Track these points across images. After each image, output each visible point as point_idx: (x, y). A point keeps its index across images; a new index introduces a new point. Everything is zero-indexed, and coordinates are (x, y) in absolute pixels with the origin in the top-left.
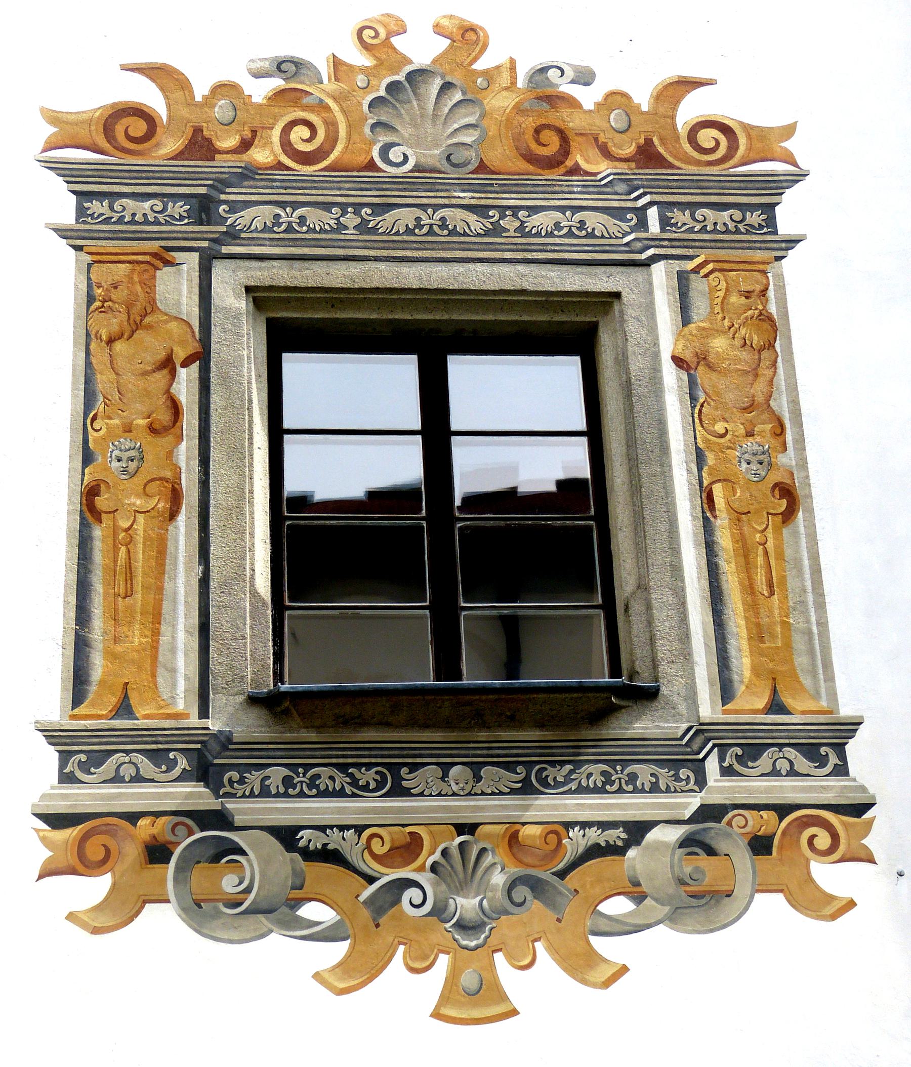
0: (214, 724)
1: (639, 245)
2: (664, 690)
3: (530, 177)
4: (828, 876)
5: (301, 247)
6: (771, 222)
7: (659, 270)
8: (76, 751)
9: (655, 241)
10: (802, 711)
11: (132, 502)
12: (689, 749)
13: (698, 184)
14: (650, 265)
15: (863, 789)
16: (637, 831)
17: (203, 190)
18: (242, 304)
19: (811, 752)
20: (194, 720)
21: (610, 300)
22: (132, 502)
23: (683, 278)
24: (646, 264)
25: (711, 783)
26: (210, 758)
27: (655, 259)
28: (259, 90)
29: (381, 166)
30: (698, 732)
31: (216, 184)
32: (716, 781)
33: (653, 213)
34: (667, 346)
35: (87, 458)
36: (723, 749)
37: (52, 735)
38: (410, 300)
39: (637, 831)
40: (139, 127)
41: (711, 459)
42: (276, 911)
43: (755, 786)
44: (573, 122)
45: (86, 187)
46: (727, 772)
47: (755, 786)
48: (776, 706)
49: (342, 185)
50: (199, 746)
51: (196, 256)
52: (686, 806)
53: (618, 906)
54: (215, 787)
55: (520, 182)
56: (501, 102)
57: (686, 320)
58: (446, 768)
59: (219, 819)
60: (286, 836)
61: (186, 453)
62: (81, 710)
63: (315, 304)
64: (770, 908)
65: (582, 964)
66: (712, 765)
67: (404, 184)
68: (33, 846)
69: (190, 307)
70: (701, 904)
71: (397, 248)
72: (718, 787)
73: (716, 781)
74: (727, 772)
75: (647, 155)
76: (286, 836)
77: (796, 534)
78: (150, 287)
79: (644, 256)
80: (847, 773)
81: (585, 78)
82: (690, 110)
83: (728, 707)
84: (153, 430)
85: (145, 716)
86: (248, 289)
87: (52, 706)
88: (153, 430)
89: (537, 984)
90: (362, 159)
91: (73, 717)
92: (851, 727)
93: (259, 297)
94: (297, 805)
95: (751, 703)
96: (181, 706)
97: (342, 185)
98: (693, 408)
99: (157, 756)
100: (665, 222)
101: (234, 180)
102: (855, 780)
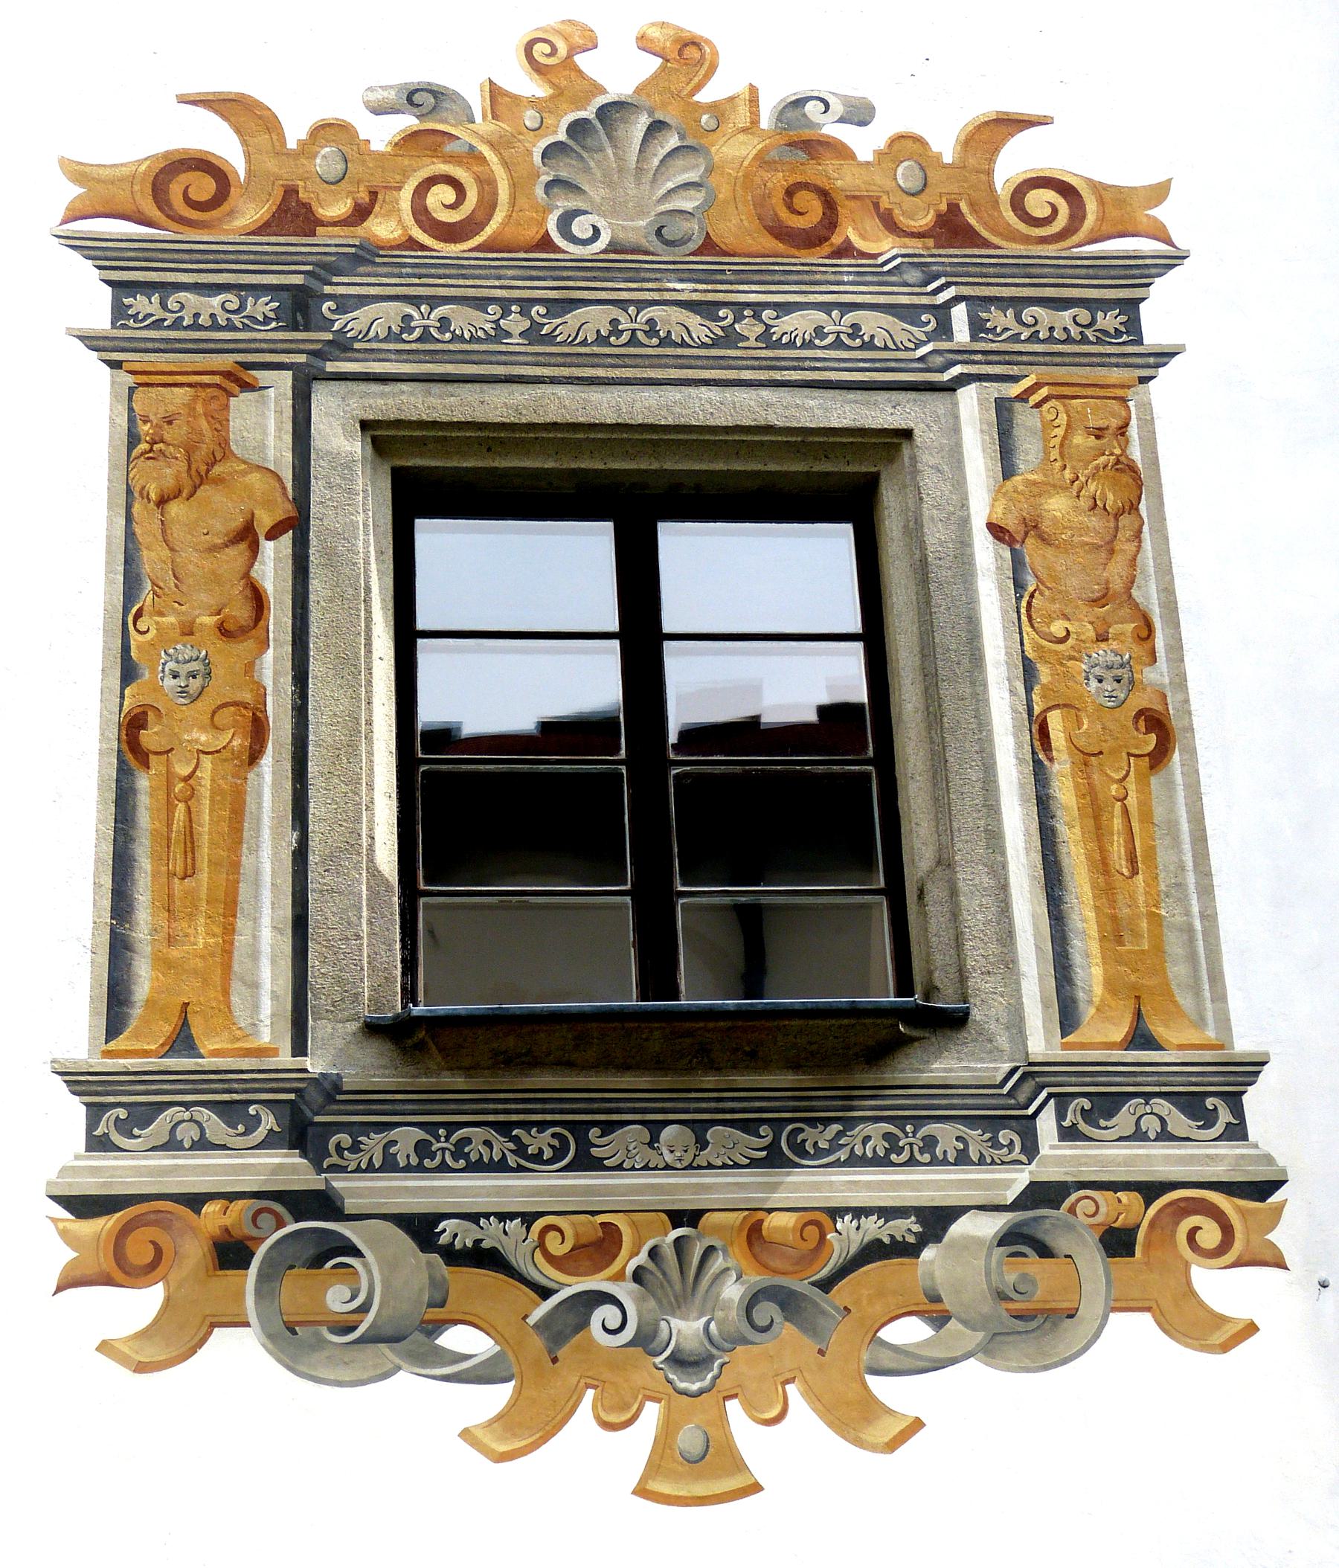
0: (315, 1065)
1: (939, 360)
2: (976, 1014)
3: (779, 260)
4: (1218, 1287)
5: (442, 363)
6: (1133, 326)
7: (968, 397)
8: (112, 1103)
9: (963, 354)
10: (1178, 1044)
11: (194, 738)
12: (1013, 1101)
13: (1026, 270)
14: (955, 390)
15: (1269, 1159)
16: (936, 1221)
17: (298, 280)
18: (355, 447)
19: (1192, 1104)
20: (285, 1059)
21: (896, 440)
22: (194, 738)
23: (1003, 409)
24: (950, 388)
25: (1044, 1150)
26: (309, 1114)
27: (963, 380)
28: (381, 133)
29: (560, 245)
30: (1025, 1076)
31: (318, 270)
32: (1052, 1147)
33: (959, 314)
34: (980, 508)
35: (129, 673)
36: (1062, 1101)
37: (77, 1081)
38: (603, 440)
39: (936, 1221)
40: (204, 187)
41: (1044, 674)
42: (406, 1339)
43: (1110, 1155)
44: (843, 179)
45: (127, 275)
46: (1069, 1134)
47: (1110, 1155)
48: (1141, 1038)
49: (502, 272)
50: (292, 1096)
51: (287, 376)
52: (1008, 1184)
53: (908, 1332)
54: (317, 1157)
55: (764, 267)
56: (736, 150)
57: (1008, 471)
58: (655, 1129)
59: (322, 1204)
60: (421, 1228)
61: (273, 666)
62: (119, 1043)
63: (463, 446)
64: (1131, 1335)
65: (855, 1417)
66: (1047, 1125)
67: (594, 270)
68: (49, 1244)
69: (279, 451)
70: (1030, 1328)
71: (584, 365)
72: (1056, 1157)
73: (1052, 1147)
74: (1069, 1134)
75: (951, 228)
76: (421, 1228)
77: (1170, 785)
78: (220, 422)
79: (946, 376)
80: (1244, 1137)
81: (860, 114)
82: (1014, 162)
83: (1070, 1038)
84: (224, 631)
85: (214, 1052)
86: (365, 425)
87: (77, 1038)
88: (224, 631)
89: (789, 1446)
90: (532, 234)
91: (107, 1054)
92: (1251, 1069)
93: (381, 436)
95: (1103, 1033)
97: (502, 272)
98: (1019, 599)
99: (231, 1111)
100: (977, 327)
101: (344, 264)
102: (1256, 1146)
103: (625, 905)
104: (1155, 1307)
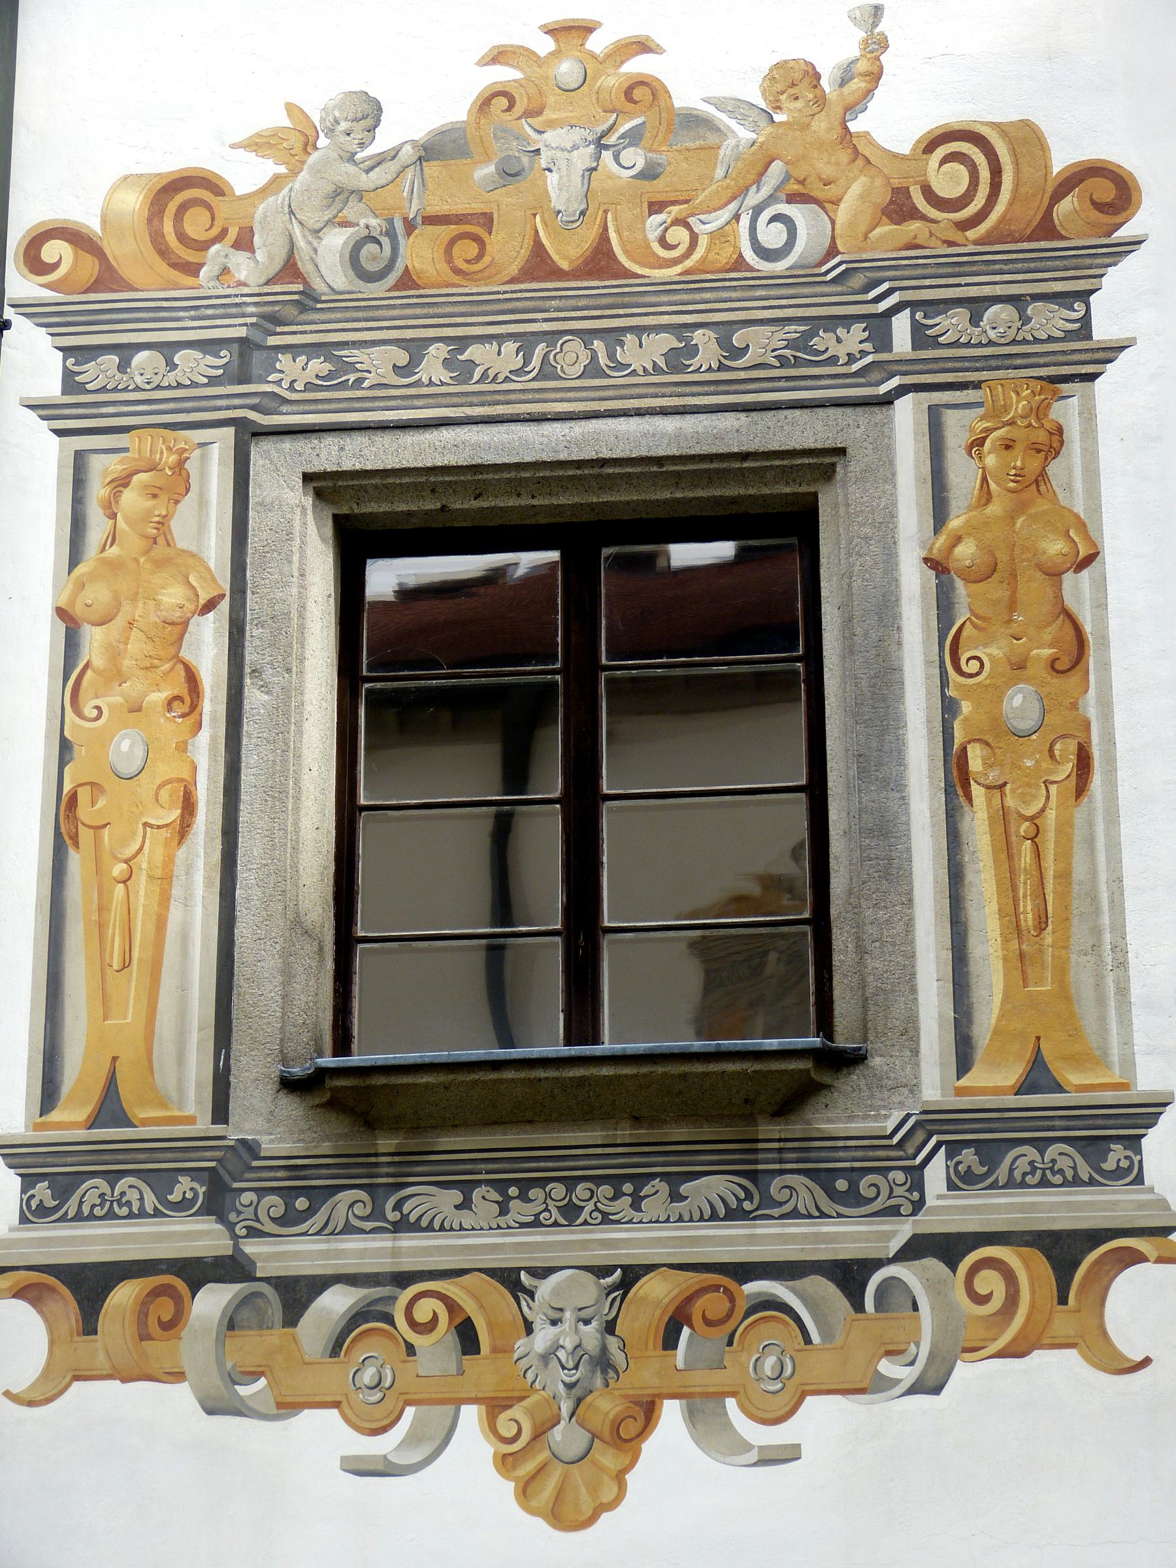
0: (233, 1133)
1: (875, 376)
2: (876, 1061)
3: (704, 277)
6: (1085, 327)
7: (905, 407)
8: (52, 1177)
10: (1079, 1084)
12: (901, 1153)
13: (158, 313)
14: (892, 403)
15: (1163, 1204)
17: (242, 332)
18: (299, 498)
19: (1093, 1147)
20: (204, 1125)
21: (825, 462)
24: (886, 401)
25: (930, 1201)
26: (227, 1178)
27: (902, 390)
29: (751, 262)
30: (918, 1124)
31: (262, 322)
32: (939, 1197)
33: (901, 325)
36: (953, 1149)
37: (17, 1155)
38: (409, 485)
40: (1105, 191)
46: (960, 1180)
48: (1038, 1077)
49: (548, 304)
50: (213, 1164)
51: (230, 432)
52: (889, 1236)
55: (627, 290)
62: (55, 1116)
63: (720, 476)
66: (936, 1174)
73: (939, 1197)
74: (960, 1180)
77: (1091, 813)
79: (883, 389)
80: (1139, 1180)
83: (963, 1082)
86: (307, 478)
90: (725, 256)
91: (38, 1127)
92: (1148, 1112)
93: (323, 486)
94: (1080, 1198)
95: (995, 1079)
96: (190, 1110)
97: (548, 304)
98: (66, 679)
99: (161, 1181)
100: (920, 336)
101: (292, 312)
102: (1151, 1190)
103: (805, 934)
104: (742, 1391)
